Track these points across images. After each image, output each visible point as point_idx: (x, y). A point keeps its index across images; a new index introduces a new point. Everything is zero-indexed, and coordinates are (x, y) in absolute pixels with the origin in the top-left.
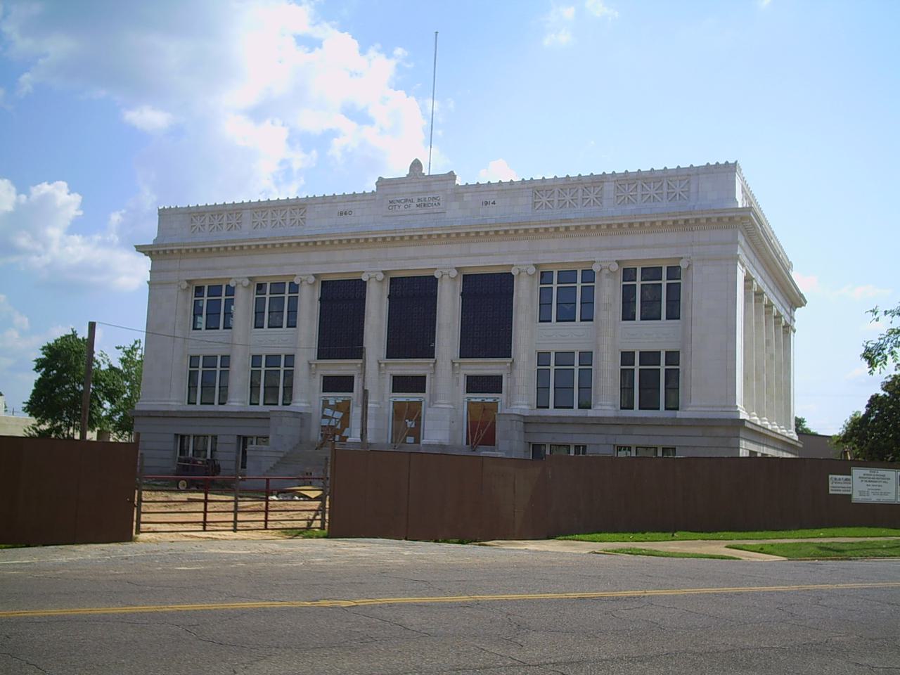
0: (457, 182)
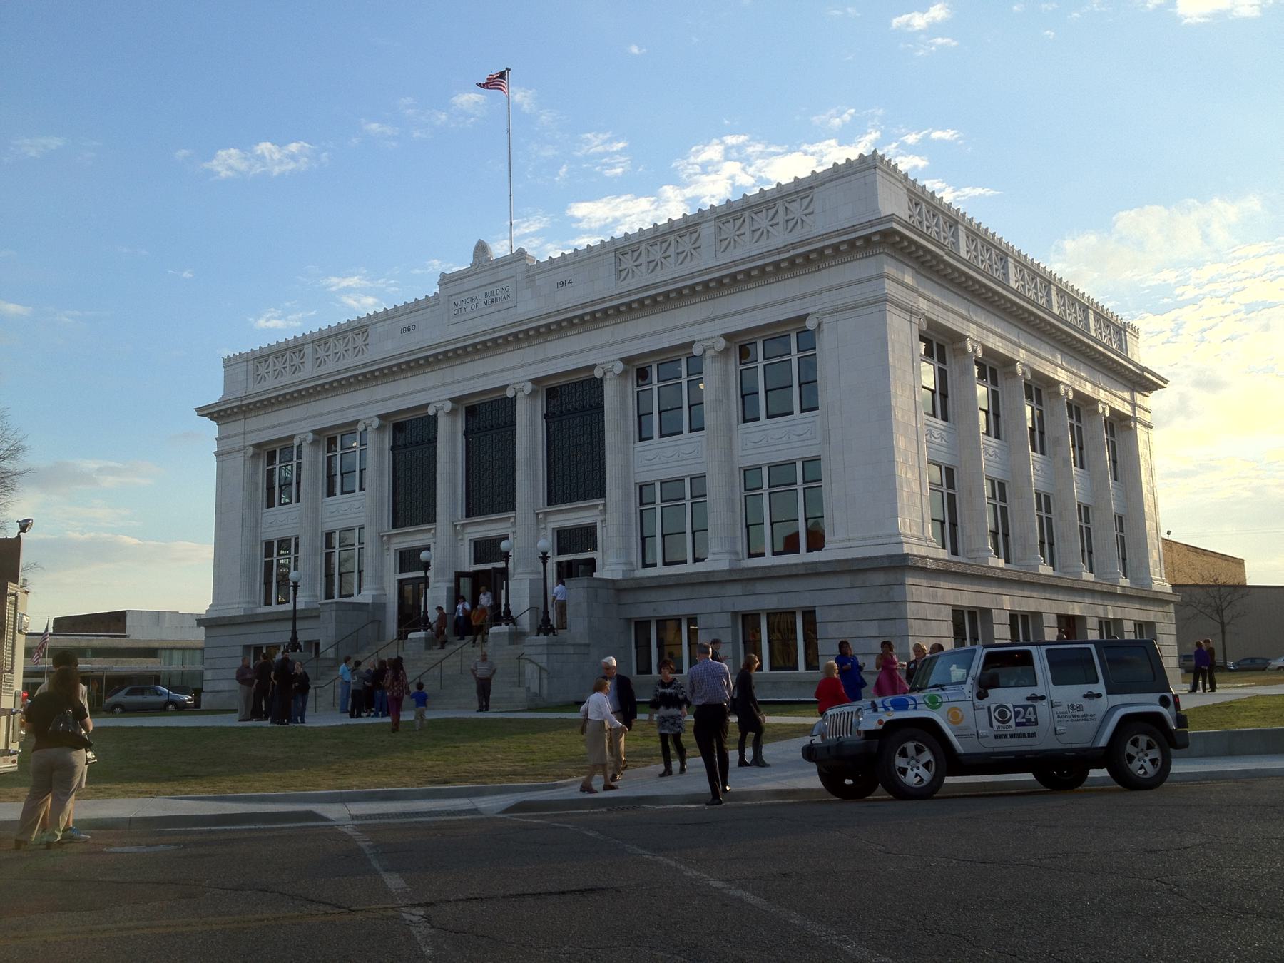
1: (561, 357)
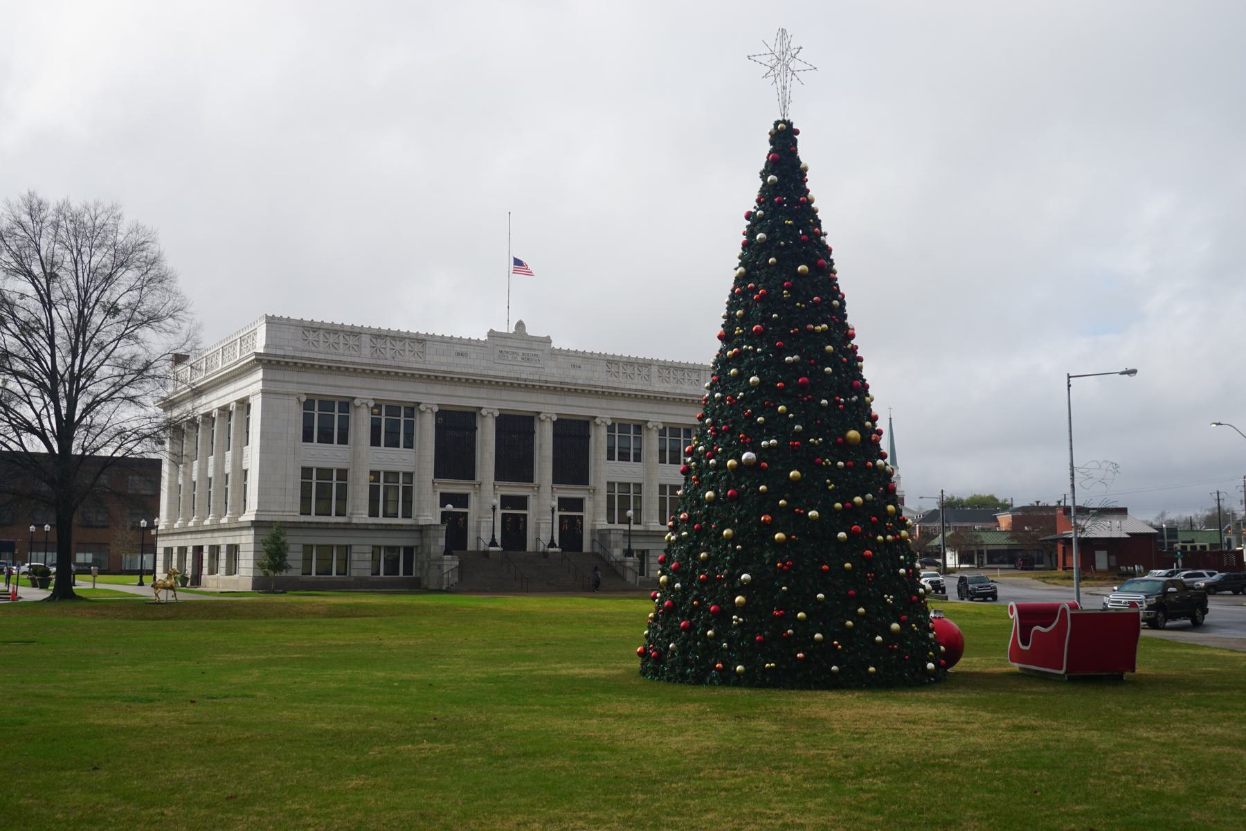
0: (553, 345)
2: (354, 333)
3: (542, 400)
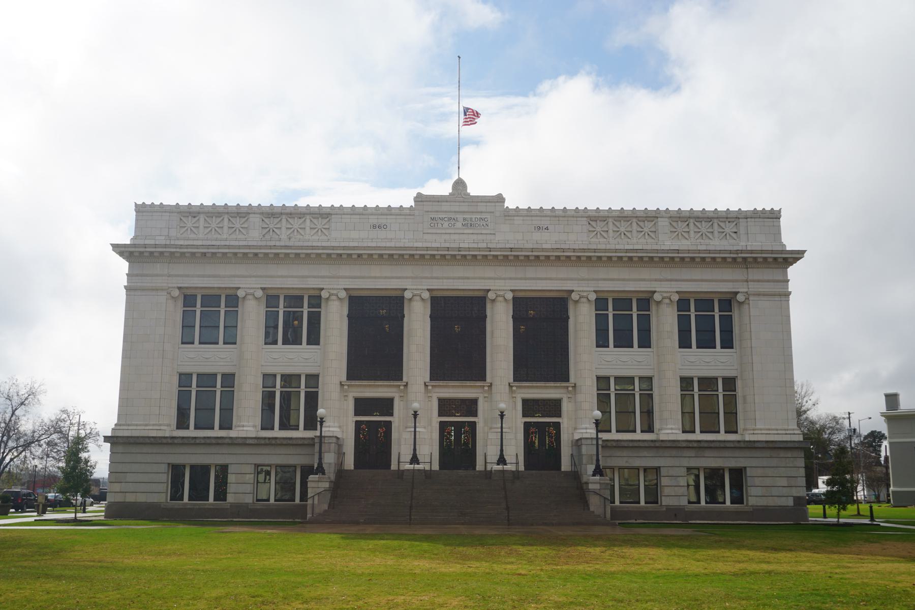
0: (506, 205)
1: (378, 280)
2: (649, 218)
3: (658, 277)
